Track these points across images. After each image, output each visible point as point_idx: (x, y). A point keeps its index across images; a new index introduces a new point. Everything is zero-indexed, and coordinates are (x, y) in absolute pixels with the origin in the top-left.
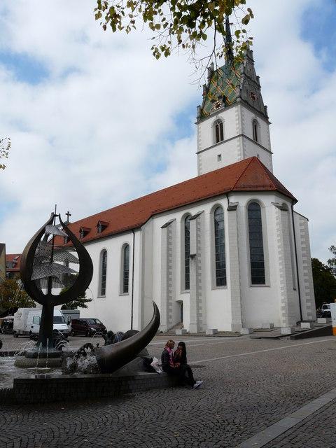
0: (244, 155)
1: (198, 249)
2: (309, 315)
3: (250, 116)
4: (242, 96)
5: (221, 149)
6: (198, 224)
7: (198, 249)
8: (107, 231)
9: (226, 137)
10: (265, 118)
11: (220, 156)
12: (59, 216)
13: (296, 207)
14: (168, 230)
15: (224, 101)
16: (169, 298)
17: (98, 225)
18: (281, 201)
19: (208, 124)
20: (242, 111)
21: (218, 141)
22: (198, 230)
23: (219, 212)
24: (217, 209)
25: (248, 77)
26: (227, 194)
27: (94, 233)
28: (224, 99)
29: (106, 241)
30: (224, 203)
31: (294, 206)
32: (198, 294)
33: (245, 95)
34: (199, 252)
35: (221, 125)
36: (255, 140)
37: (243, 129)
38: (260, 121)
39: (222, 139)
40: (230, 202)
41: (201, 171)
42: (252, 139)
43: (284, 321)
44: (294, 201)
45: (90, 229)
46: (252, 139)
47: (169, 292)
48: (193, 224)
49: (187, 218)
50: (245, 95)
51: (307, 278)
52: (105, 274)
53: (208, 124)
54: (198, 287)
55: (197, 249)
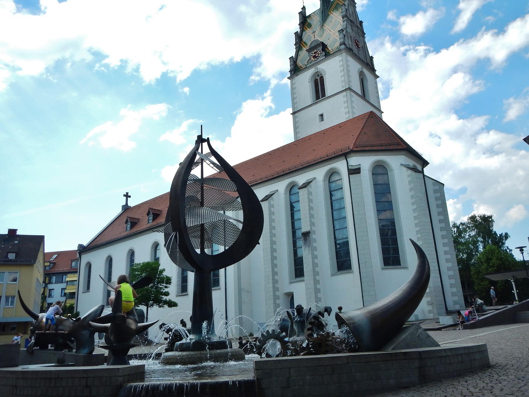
0: (353, 113)
1: (312, 224)
2: (455, 303)
3: (355, 66)
4: (347, 43)
5: (323, 106)
6: (310, 194)
7: (312, 224)
8: (136, 229)
9: (328, 93)
10: (373, 70)
11: (322, 115)
12: (208, 140)
13: (427, 171)
14: (269, 203)
15: (323, 50)
16: (275, 289)
17: (148, 214)
18: (411, 163)
19: (306, 77)
20: (347, 61)
21: (318, 98)
22: (310, 201)
23: (335, 178)
24: (332, 173)
25: (351, 21)
26: (345, 155)
27: (144, 224)
28: (324, 47)
29: (108, 247)
30: (341, 166)
31: (425, 170)
32: (316, 282)
33: (348, 42)
34: (313, 228)
35: (322, 79)
36: (364, 96)
37: (349, 81)
38: (366, 72)
39: (324, 95)
40: (350, 164)
41: (298, 135)
42: (360, 94)
43: (430, 312)
44: (425, 163)
45: (139, 219)
46: (360, 94)
47: (275, 282)
48: (303, 194)
49: (292, 188)
50: (348, 42)
51: (449, 257)
52: (90, 273)
53: (306, 77)
54: (316, 274)
55: (311, 226)
